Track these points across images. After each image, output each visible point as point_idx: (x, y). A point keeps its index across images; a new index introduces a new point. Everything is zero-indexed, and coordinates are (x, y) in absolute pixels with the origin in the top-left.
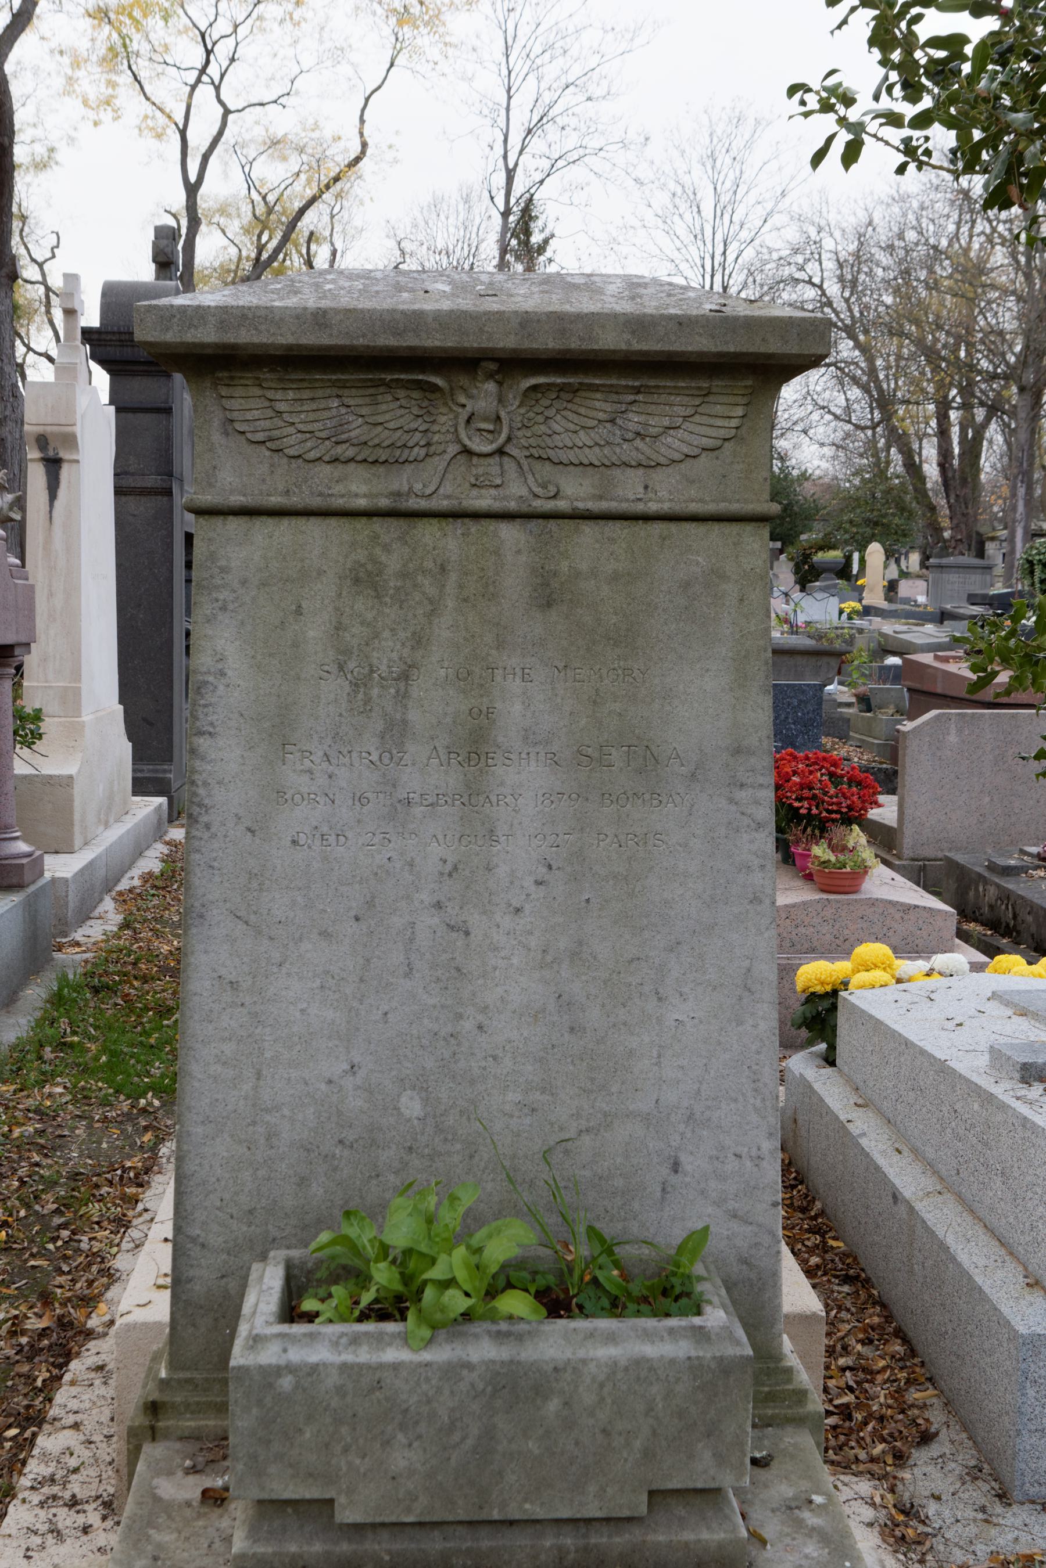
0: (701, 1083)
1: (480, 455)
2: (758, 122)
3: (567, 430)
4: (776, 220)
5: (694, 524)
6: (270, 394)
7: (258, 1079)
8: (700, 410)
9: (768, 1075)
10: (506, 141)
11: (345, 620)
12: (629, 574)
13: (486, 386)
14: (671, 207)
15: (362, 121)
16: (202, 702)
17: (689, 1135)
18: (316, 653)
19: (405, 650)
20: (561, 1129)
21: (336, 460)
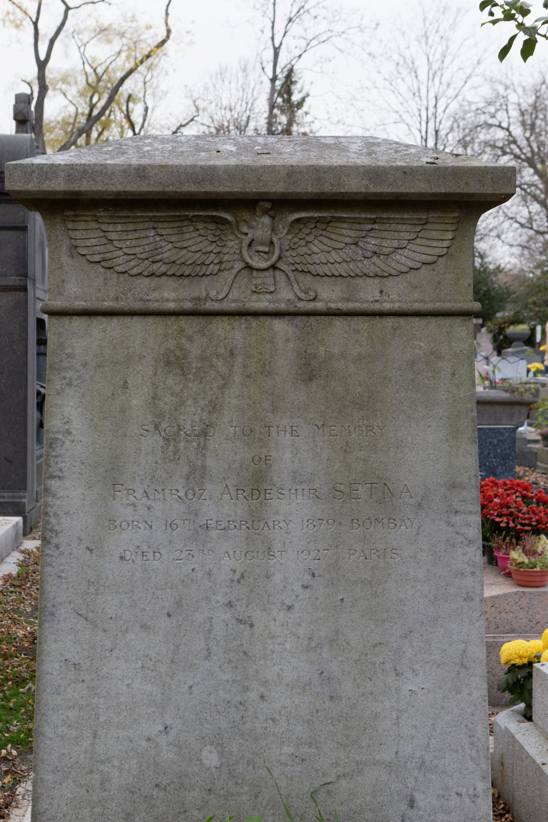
0: (429, 738)
1: (258, 270)
2: (459, 10)
3: (322, 251)
4: (475, 81)
5: (417, 319)
6: (104, 227)
7: (95, 738)
8: (420, 235)
9: (481, 730)
10: (273, 27)
11: (159, 392)
12: (369, 356)
13: (263, 219)
14: (395, 72)
15: (167, 14)
16: (54, 454)
17: (421, 779)
18: (138, 416)
19: (204, 414)
20: (324, 775)
21: (153, 274)
